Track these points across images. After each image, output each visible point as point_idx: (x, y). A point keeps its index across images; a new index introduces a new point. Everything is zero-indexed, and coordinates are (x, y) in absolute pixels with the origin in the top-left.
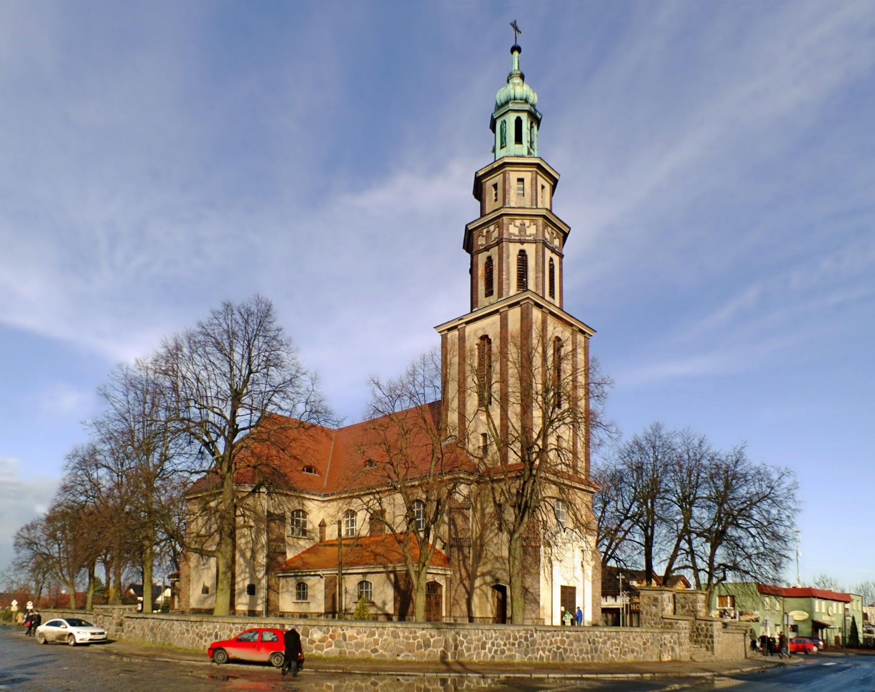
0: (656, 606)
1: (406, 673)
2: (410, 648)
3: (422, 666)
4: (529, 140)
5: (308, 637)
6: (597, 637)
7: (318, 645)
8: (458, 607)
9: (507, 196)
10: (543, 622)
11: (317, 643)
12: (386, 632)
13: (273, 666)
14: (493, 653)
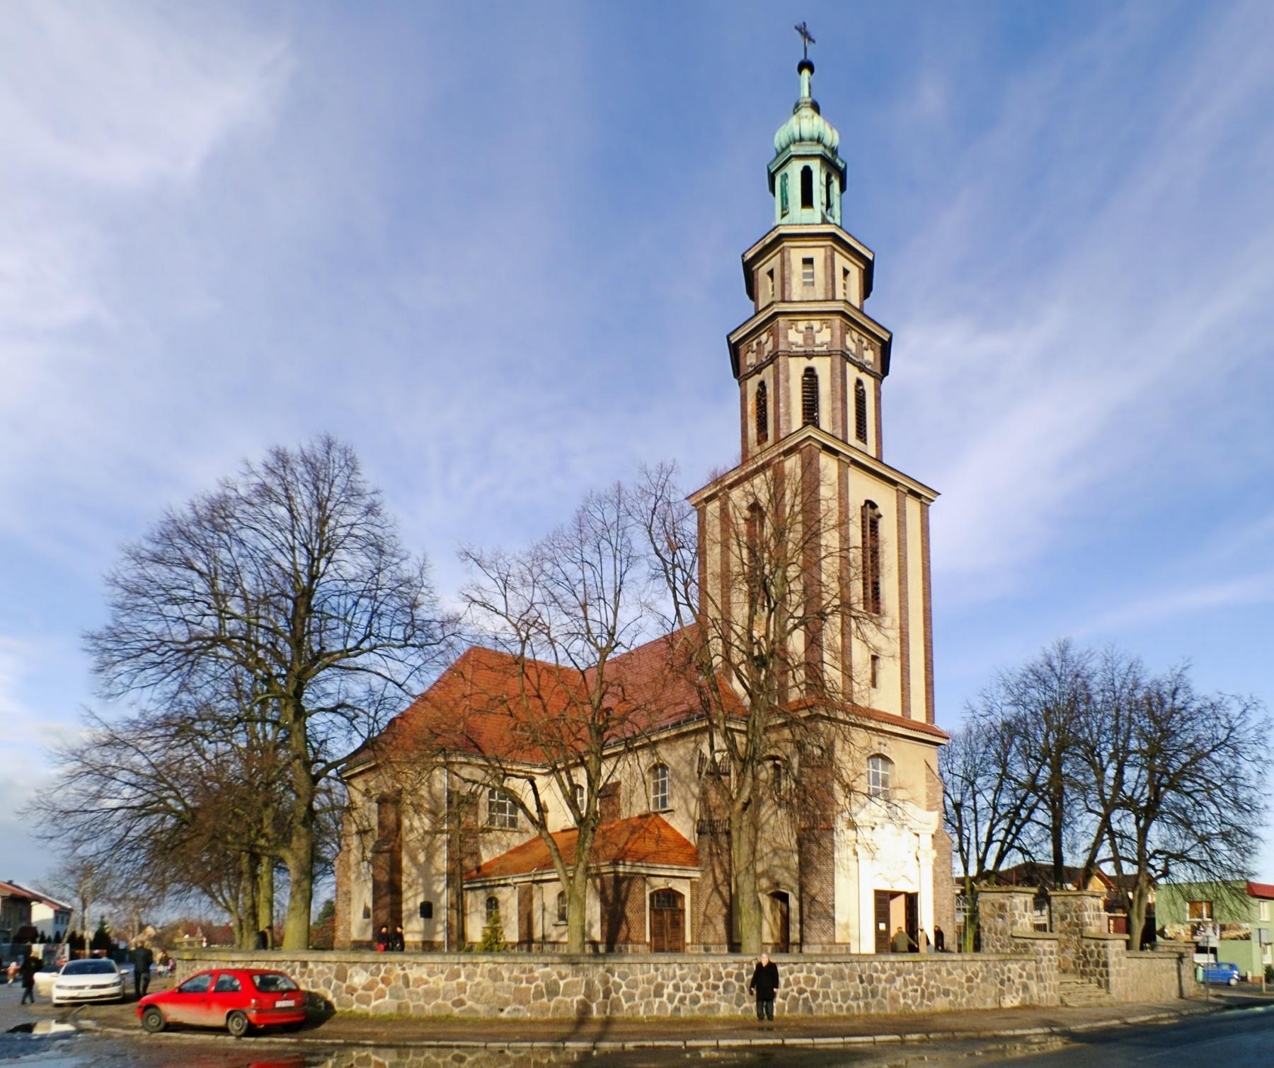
0: (1002, 917)
1: (455, 1043)
3: (504, 1029)
4: (824, 200)
5: (345, 982)
6: (876, 971)
8: (711, 928)
9: (787, 286)
10: (848, 949)
11: (360, 992)
12: (479, 971)
13: (231, 1035)
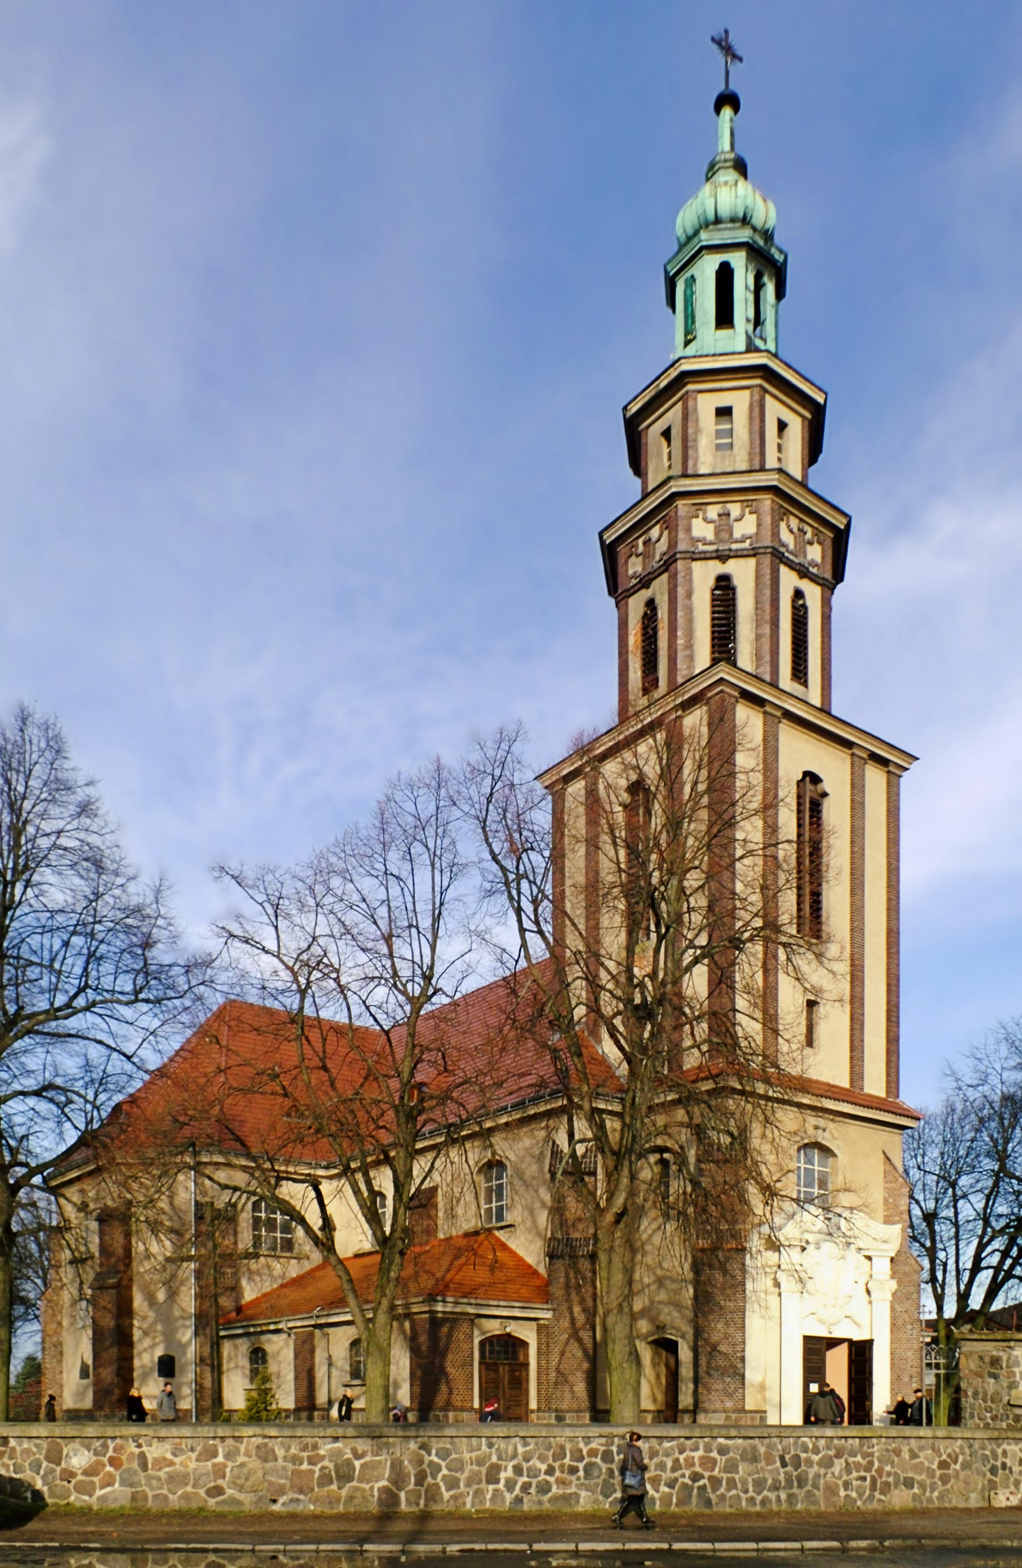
0: (995, 1377)
1: (211, 1546)
2: (301, 1485)
3: (277, 1526)
5: (59, 1464)
7: (82, 1482)
9: (691, 452)
10: (763, 1419)
11: (80, 1477)
12: (242, 1448)
14: (517, 1490)
